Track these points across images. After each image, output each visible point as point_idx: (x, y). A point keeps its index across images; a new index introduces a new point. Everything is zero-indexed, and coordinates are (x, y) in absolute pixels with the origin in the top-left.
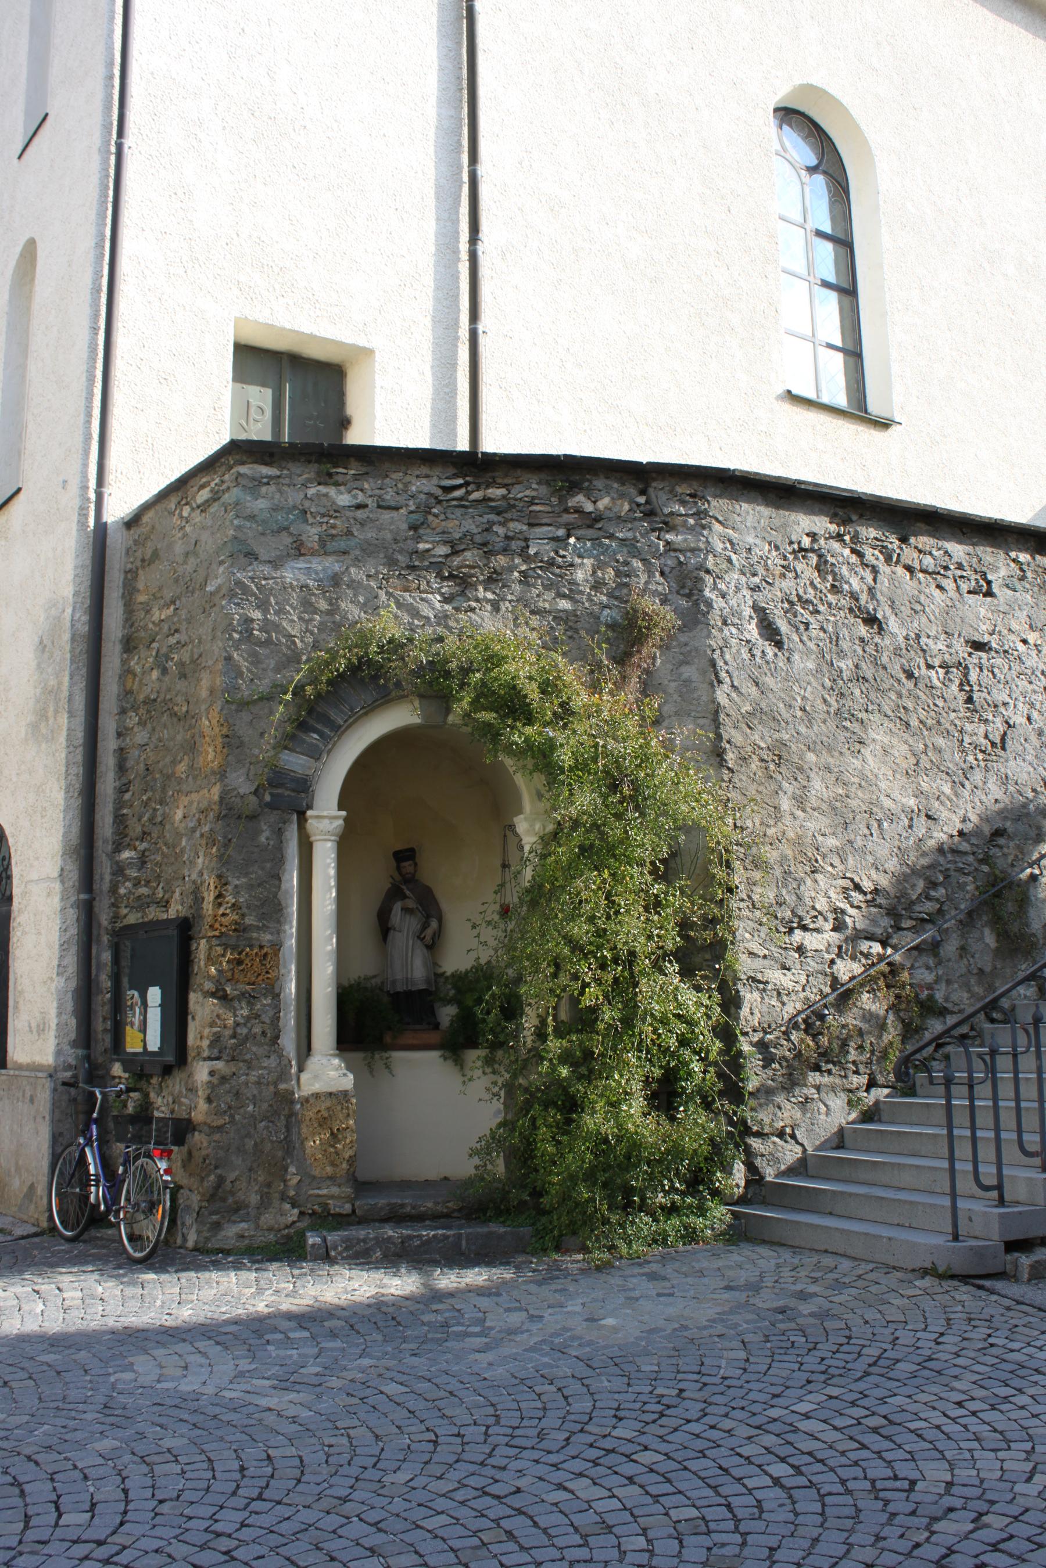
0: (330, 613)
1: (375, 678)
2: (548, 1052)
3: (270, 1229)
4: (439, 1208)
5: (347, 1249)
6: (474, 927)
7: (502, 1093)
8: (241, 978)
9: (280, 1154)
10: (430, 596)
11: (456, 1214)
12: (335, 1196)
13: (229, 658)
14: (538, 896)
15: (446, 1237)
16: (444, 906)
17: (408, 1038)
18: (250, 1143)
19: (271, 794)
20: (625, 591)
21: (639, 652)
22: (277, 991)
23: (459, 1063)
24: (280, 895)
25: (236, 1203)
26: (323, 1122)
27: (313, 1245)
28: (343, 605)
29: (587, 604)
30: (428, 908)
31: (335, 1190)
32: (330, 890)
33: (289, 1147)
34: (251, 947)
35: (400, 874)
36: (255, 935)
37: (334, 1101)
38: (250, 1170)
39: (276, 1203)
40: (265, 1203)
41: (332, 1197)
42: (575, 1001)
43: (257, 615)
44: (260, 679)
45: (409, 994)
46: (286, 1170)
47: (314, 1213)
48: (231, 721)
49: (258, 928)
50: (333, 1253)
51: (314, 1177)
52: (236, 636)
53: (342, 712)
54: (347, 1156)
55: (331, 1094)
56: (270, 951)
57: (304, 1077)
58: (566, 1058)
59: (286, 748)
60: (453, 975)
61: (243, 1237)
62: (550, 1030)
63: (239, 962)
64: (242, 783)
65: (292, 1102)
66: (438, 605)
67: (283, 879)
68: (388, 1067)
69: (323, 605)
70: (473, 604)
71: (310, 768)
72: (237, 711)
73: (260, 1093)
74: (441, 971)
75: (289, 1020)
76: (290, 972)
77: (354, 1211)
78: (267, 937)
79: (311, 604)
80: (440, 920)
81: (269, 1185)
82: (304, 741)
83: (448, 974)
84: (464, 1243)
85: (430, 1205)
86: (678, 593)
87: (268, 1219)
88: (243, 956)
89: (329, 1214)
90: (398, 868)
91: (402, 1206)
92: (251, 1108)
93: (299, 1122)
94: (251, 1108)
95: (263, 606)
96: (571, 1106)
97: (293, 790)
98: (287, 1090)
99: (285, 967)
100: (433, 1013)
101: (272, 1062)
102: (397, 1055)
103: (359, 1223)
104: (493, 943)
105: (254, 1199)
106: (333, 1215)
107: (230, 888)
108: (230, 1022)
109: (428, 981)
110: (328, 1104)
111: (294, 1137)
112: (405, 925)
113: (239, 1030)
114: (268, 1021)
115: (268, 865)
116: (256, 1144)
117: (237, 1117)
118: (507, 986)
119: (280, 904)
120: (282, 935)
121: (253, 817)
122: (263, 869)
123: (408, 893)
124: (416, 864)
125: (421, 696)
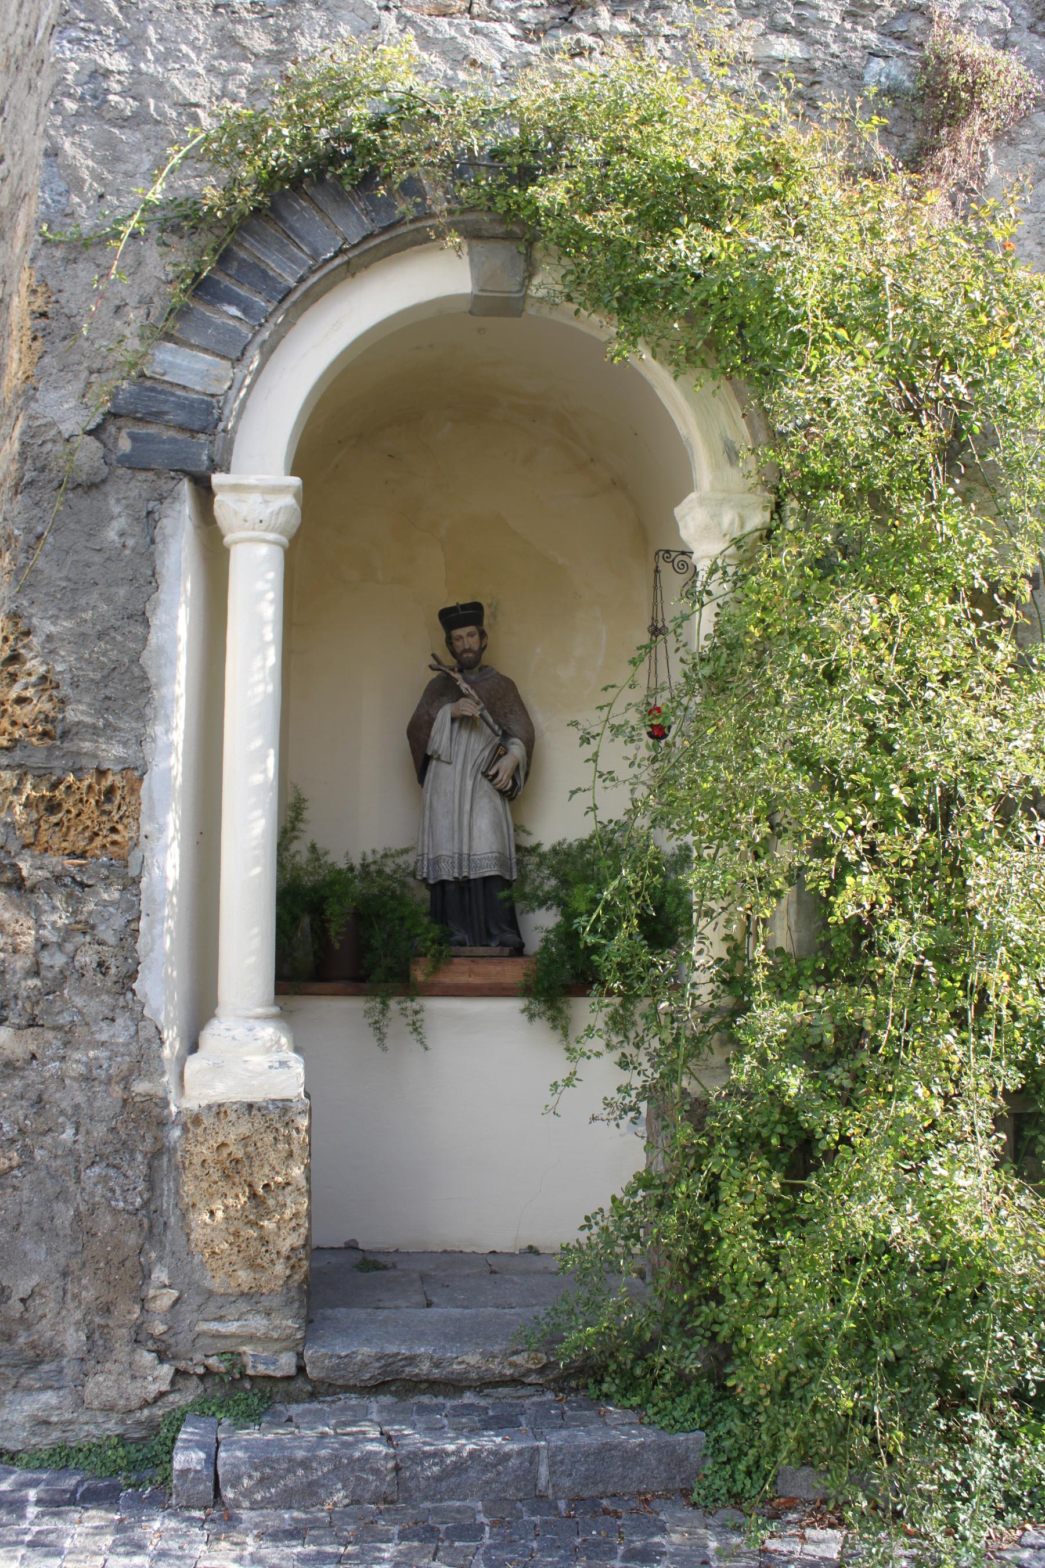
0: (274, 58)
1: (367, 182)
2: (754, 1033)
3: (108, 1409)
4: (495, 1366)
5: (263, 1482)
6: (585, 740)
7: (643, 1106)
8: (56, 842)
9: (132, 1240)
10: (496, 26)
11: (533, 1378)
12: (261, 1336)
13: (53, 153)
14: (723, 672)
15: (501, 1458)
16: (540, 719)
17: (460, 972)
18: (65, 1214)
19: (133, 437)
20: (918, 22)
21: (953, 141)
22: (133, 872)
23: (560, 1022)
24: (145, 657)
25: (33, 1346)
26: (232, 1169)
27: (184, 1472)
28: (304, 42)
29: (835, 48)
30: (505, 714)
31: (257, 1324)
32: (264, 646)
33: (152, 1224)
34: (78, 771)
35: (454, 654)
36: (87, 746)
37: (259, 1122)
38: (65, 1274)
39: (121, 1350)
40: (97, 1348)
41: (251, 1338)
42: (815, 907)
43: (118, 62)
44: (118, 193)
45: (464, 885)
46: (147, 1276)
47: (209, 1372)
48: (52, 283)
49: (95, 731)
50: (229, 1494)
51: (210, 1294)
52: (71, 106)
53: (293, 259)
54: (285, 1247)
55: (250, 1106)
56: (119, 782)
57: (194, 1064)
58: (801, 1047)
59: (169, 337)
60: (555, 851)
61: (47, 1423)
62: (760, 976)
63: (53, 807)
64: (68, 411)
65: (162, 1124)
66: (510, 44)
67: (154, 622)
68: (416, 1028)
69: (260, 42)
70: (588, 40)
71: (219, 380)
72: (67, 261)
73: (90, 1101)
74: (529, 842)
75: (164, 939)
76: (162, 829)
77: (301, 1369)
78: (112, 752)
79: (235, 41)
80: (530, 744)
81: (107, 1310)
82: (208, 323)
83: (546, 848)
84: (543, 1471)
85: (473, 1359)
86: (1032, 29)
87: (102, 1386)
88: (59, 793)
89: (243, 1375)
90: (449, 641)
91: (411, 1360)
92: (68, 1135)
93: (180, 1169)
94: (68, 1135)
95: (131, 44)
96: (801, 1155)
97: (181, 428)
98: (150, 1097)
99: (152, 818)
100: (513, 924)
101: (120, 1032)
102: (437, 1006)
103: (313, 1396)
104: (624, 772)
105: (73, 1340)
106: (251, 1378)
107: (35, 641)
108: (28, 940)
109: (502, 860)
110: (244, 1129)
111: (166, 1203)
112: (459, 750)
113: (46, 959)
114: (112, 940)
115: (122, 592)
116: (78, 1214)
117: (39, 1154)
118: (655, 870)
119: (145, 678)
120: (147, 747)
121: (92, 486)
122: (109, 600)
123: (464, 686)
124: (483, 634)
125: (473, 234)
